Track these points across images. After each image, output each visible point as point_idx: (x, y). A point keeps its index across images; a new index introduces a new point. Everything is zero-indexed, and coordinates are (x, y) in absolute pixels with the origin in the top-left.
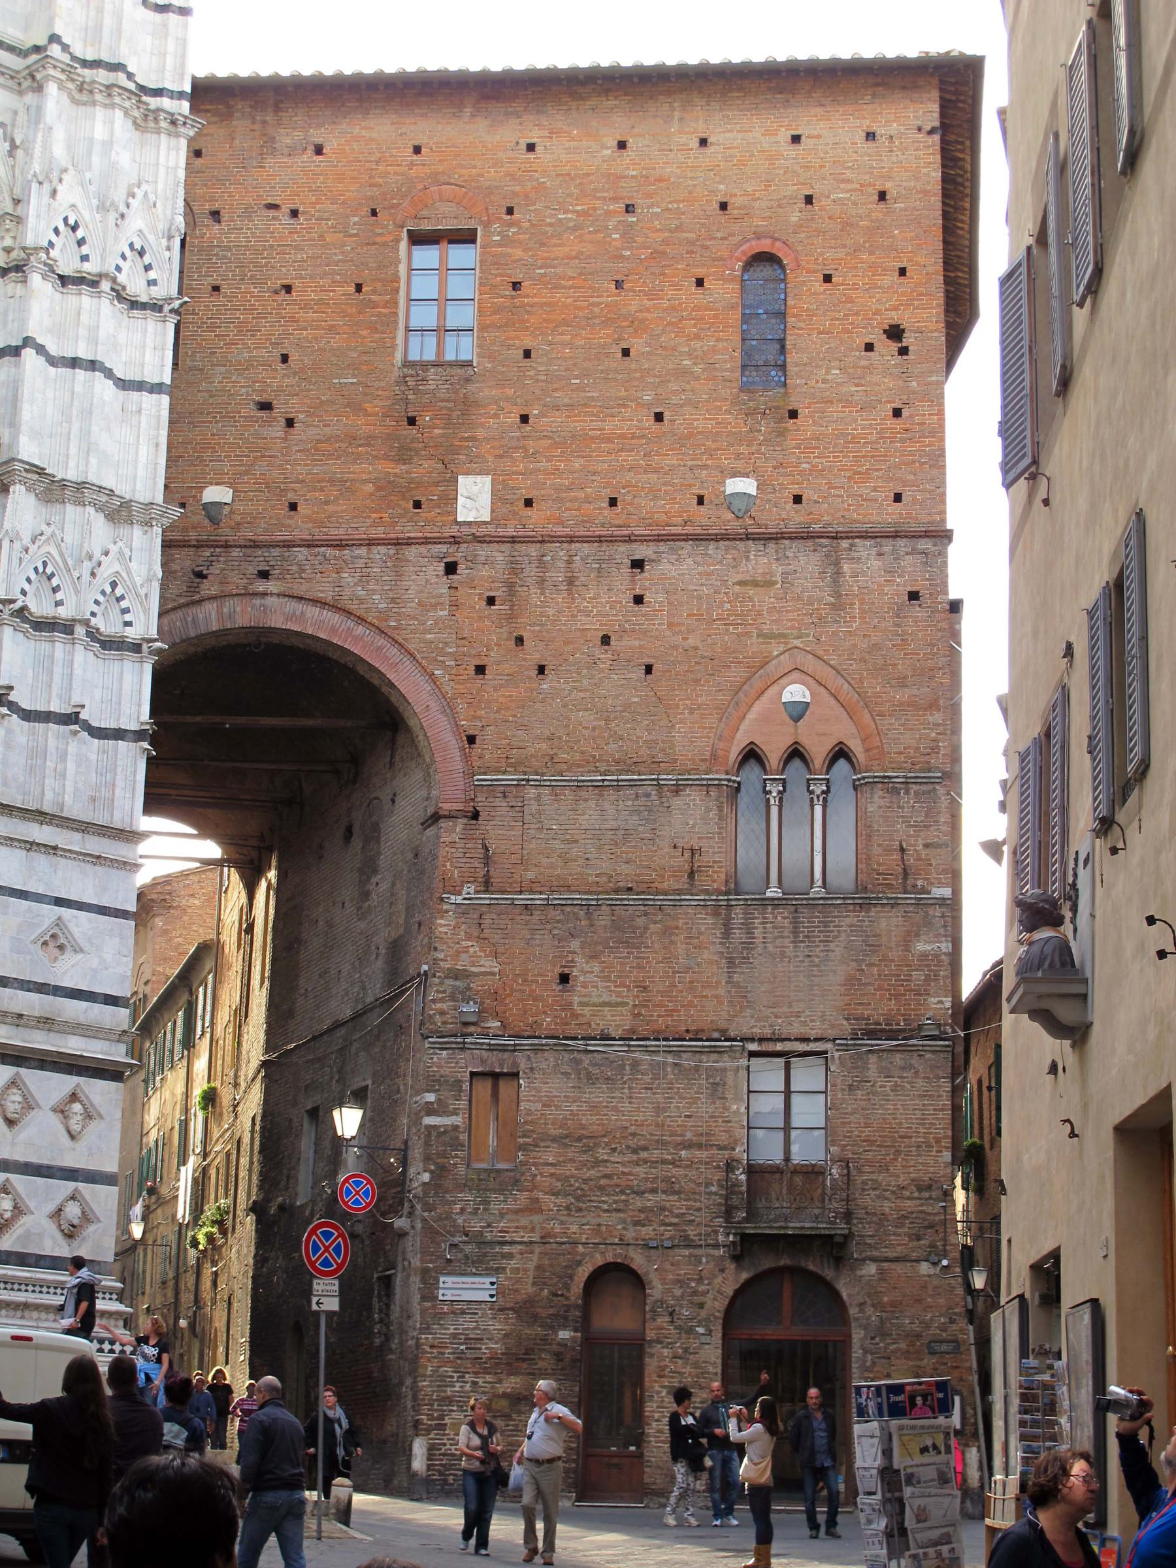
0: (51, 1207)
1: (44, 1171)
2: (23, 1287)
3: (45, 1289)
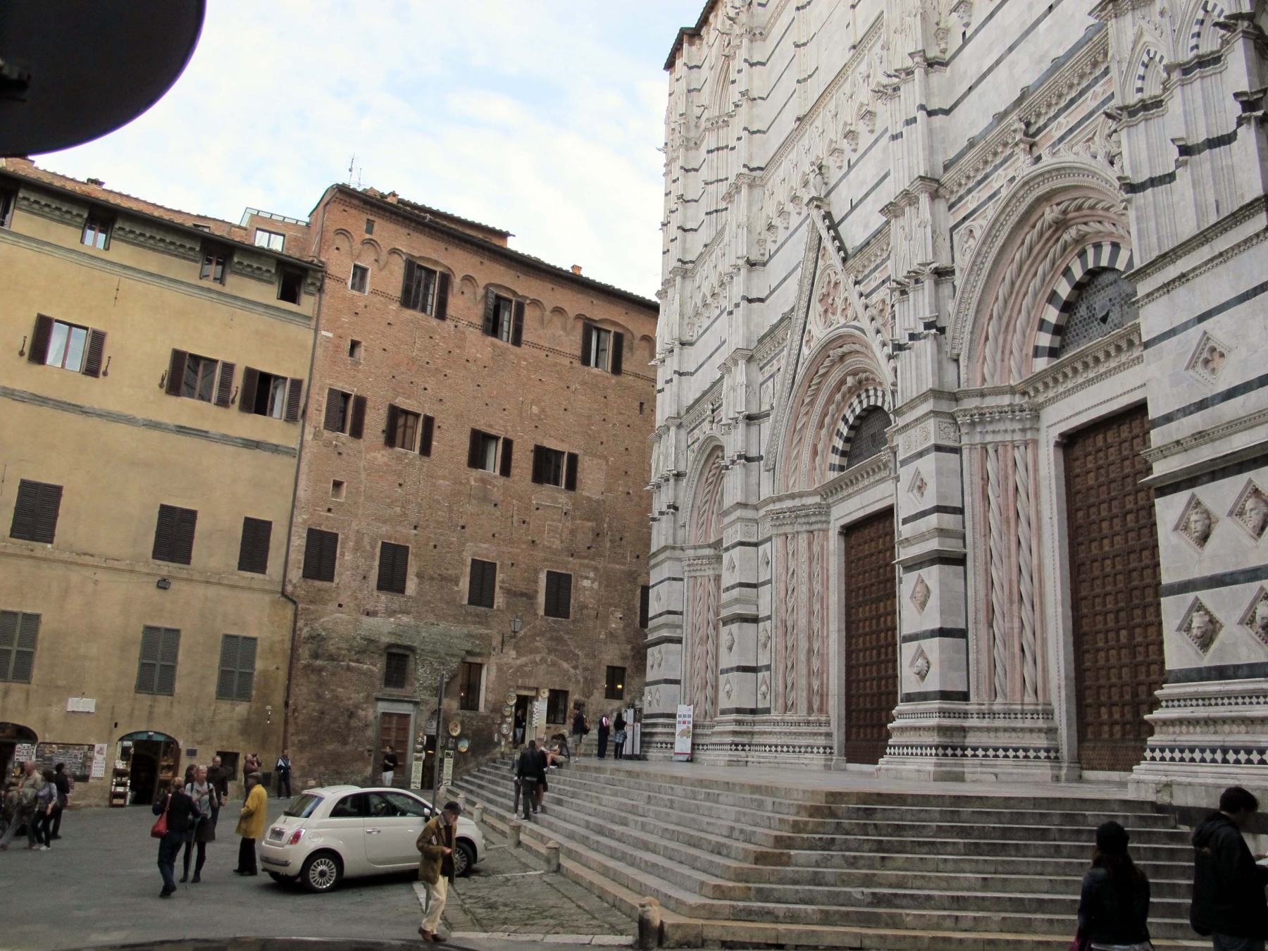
0: (1240, 613)
1: (1228, 580)
2: (1220, 701)
3: (1240, 700)
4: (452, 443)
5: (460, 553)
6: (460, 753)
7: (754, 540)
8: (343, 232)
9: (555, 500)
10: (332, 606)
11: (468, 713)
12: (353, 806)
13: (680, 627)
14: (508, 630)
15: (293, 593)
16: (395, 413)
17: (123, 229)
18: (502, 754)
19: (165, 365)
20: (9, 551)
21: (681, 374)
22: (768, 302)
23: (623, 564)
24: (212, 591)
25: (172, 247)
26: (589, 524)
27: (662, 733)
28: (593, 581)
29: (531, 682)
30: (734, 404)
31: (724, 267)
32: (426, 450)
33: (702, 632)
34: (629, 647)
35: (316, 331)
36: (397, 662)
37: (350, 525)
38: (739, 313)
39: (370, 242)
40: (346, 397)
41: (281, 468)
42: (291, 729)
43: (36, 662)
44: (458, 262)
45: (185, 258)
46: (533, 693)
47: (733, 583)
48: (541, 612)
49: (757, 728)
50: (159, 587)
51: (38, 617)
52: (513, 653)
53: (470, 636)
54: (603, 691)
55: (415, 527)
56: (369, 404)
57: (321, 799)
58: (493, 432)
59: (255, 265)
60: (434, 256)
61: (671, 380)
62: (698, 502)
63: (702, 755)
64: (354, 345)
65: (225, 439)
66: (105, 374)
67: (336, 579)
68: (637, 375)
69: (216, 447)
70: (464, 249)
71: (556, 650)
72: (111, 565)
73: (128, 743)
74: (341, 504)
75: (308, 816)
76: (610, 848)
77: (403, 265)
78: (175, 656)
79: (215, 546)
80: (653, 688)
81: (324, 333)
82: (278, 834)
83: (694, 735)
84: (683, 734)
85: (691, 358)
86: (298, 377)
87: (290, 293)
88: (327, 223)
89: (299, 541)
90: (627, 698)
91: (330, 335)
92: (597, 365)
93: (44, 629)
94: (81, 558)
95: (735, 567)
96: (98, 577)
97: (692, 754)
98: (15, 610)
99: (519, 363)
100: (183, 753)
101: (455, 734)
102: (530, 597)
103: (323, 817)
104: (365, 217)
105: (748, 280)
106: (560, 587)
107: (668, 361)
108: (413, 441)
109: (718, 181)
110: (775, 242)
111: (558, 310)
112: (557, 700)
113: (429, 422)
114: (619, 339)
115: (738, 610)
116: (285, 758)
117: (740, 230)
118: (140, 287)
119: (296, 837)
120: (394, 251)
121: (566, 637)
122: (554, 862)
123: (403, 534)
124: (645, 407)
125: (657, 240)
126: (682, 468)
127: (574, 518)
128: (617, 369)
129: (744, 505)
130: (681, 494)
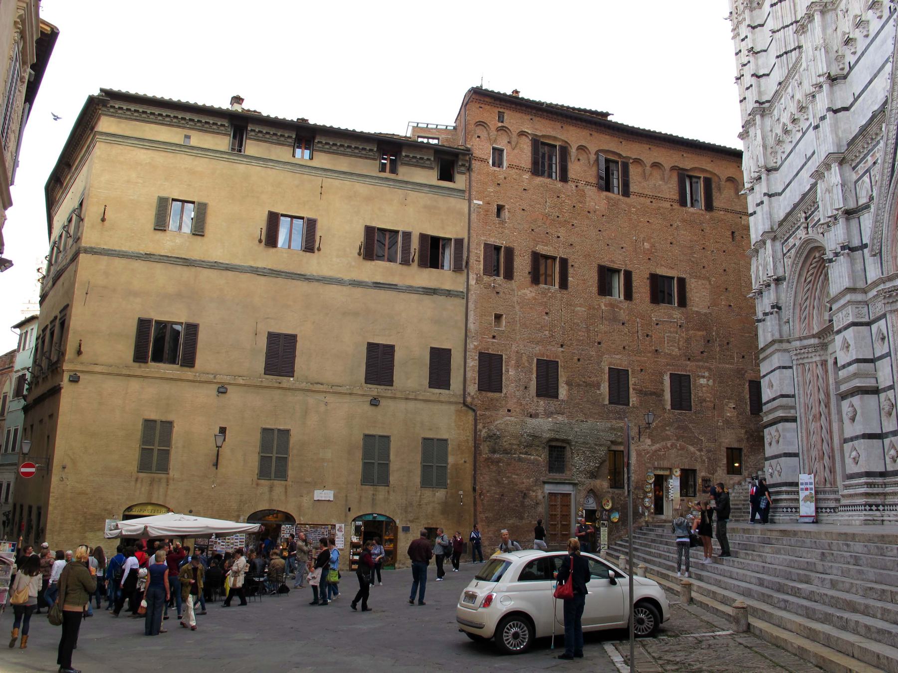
4: (584, 277)
5: (599, 363)
6: (613, 522)
7: (866, 319)
8: (481, 124)
9: (671, 316)
10: (503, 412)
11: (616, 491)
12: (539, 570)
13: (794, 408)
14: (643, 424)
15: (471, 404)
16: (537, 259)
17: (321, 142)
18: (646, 522)
19: (359, 237)
20: (264, 384)
21: (770, 196)
22: (852, 109)
23: (732, 364)
24: (411, 405)
25: (357, 151)
26: (700, 333)
27: (785, 499)
28: (709, 379)
29: (666, 464)
30: (831, 200)
31: (808, 88)
32: (564, 284)
33: (815, 411)
34: (743, 431)
35: (470, 200)
36: (557, 452)
37: (510, 348)
38: (826, 126)
39: (503, 129)
40: (497, 249)
41: (454, 307)
42: (479, 509)
43: (290, 464)
44: (573, 137)
45: (366, 158)
46: (667, 473)
47: (848, 360)
48: (668, 407)
49: (889, 490)
50: (372, 405)
51: (288, 431)
52: (649, 441)
53: (612, 429)
54: (725, 468)
55: (562, 346)
56: (516, 253)
57: (509, 563)
58: (615, 266)
59: (418, 157)
60: (553, 134)
61: (762, 203)
62: (799, 300)
63: (824, 517)
64: (500, 208)
65: (411, 290)
66: (319, 249)
67: (504, 391)
68: (726, 210)
69: (403, 296)
70: (575, 125)
71: (683, 437)
72: (335, 390)
73: (360, 523)
74: (503, 332)
75: (498, 580)
76: (807, 608)
77: (530, 143)
78: (388, 456)
79: (410, 372)
80: (774, 462)
81: (475, 202)
82: (472, 597)
83: (816, 499)
84: (806, 499)
85: (777, 181)
86: (460, 237)
87: (446, 175)
88: (468, 118)
89: (473, 363)
90: (745, 473)
91: (481, 203)
92: (692, 205)
93: (293, 440)
94: (314, 388)
95: (847, 347)
96: (327, 399)
97: (817, 516)
98: (273, 427)
99: (630, 211)
100: (400, 530)
101: (607, 508)
102: (659, 394)
103: (511, 581)
104: (496, 110)
105: (831, 93)
106: (682, 387)
107: (757, 188)
108: (552, 276)
109: (784, 28)
110: (854, 53)
111: (656, 165)
112: (687, 476)
113: (564, 262)
114: (708, 182)
115: (857, 383)
116: (476, 530)
117: (817, 53)
118: (337, 183)
119: (488, 600)
120: (522, 134)
121: (690, 426)
122: (743, 622)
123: (553, 352)
124: (739, 233)
125: (735, 92)
126: (780, 273)
127: (687, 330)
128: (709, 207)
129: (849, 290)
130: (783, 296)
